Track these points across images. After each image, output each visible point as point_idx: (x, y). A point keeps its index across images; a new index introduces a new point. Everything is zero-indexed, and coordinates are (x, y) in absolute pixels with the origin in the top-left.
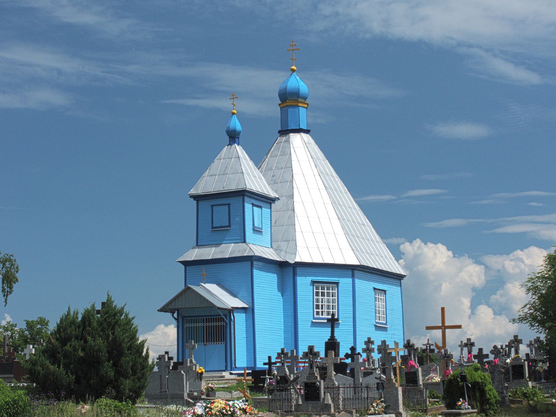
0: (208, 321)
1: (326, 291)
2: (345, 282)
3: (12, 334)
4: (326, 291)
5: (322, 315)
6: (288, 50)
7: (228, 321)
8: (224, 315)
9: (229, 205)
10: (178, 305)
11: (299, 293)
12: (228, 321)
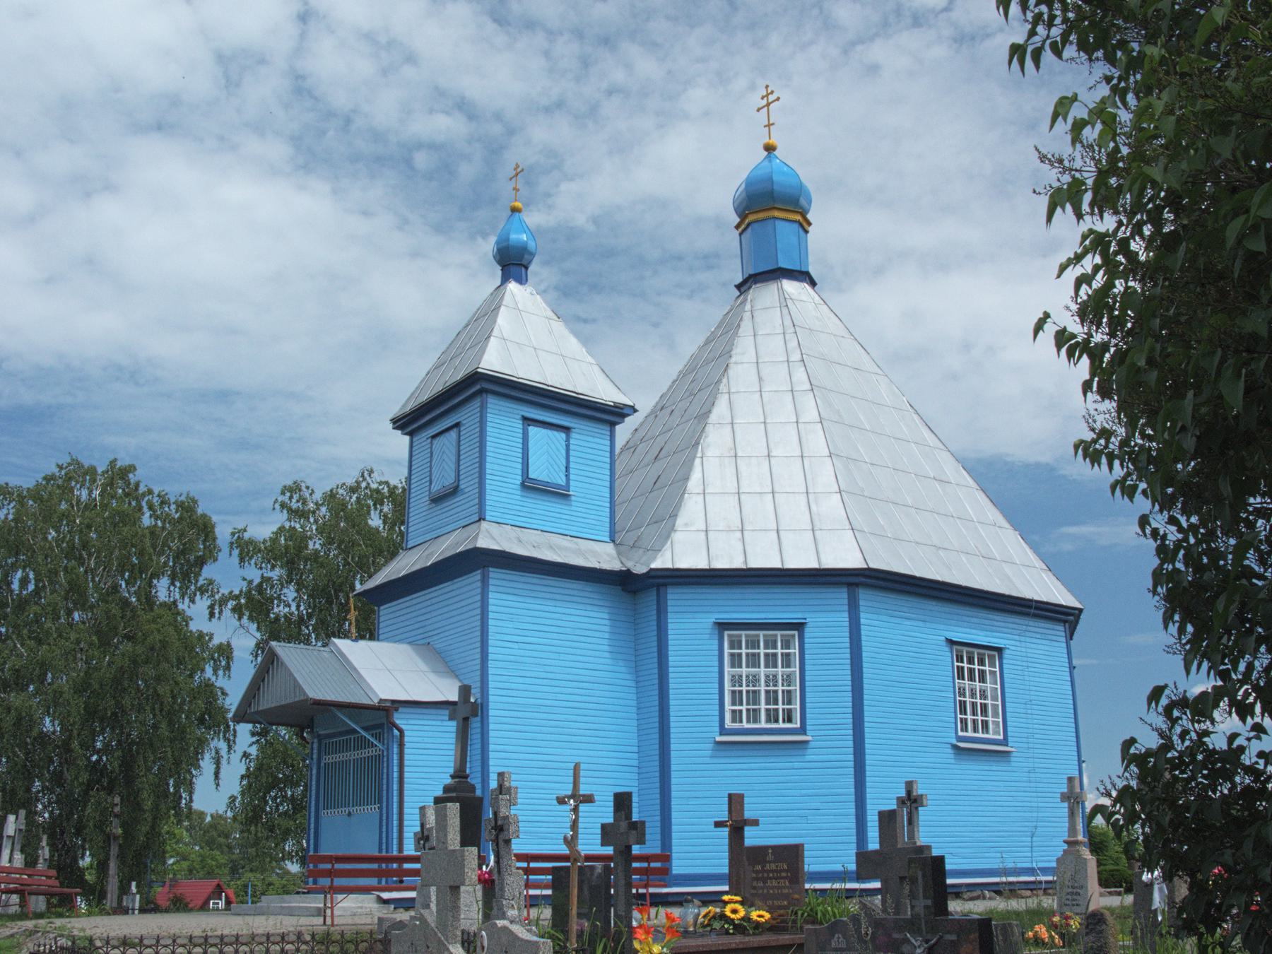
2: (826, 620)
6: (758, 110)
9: (457, 425)
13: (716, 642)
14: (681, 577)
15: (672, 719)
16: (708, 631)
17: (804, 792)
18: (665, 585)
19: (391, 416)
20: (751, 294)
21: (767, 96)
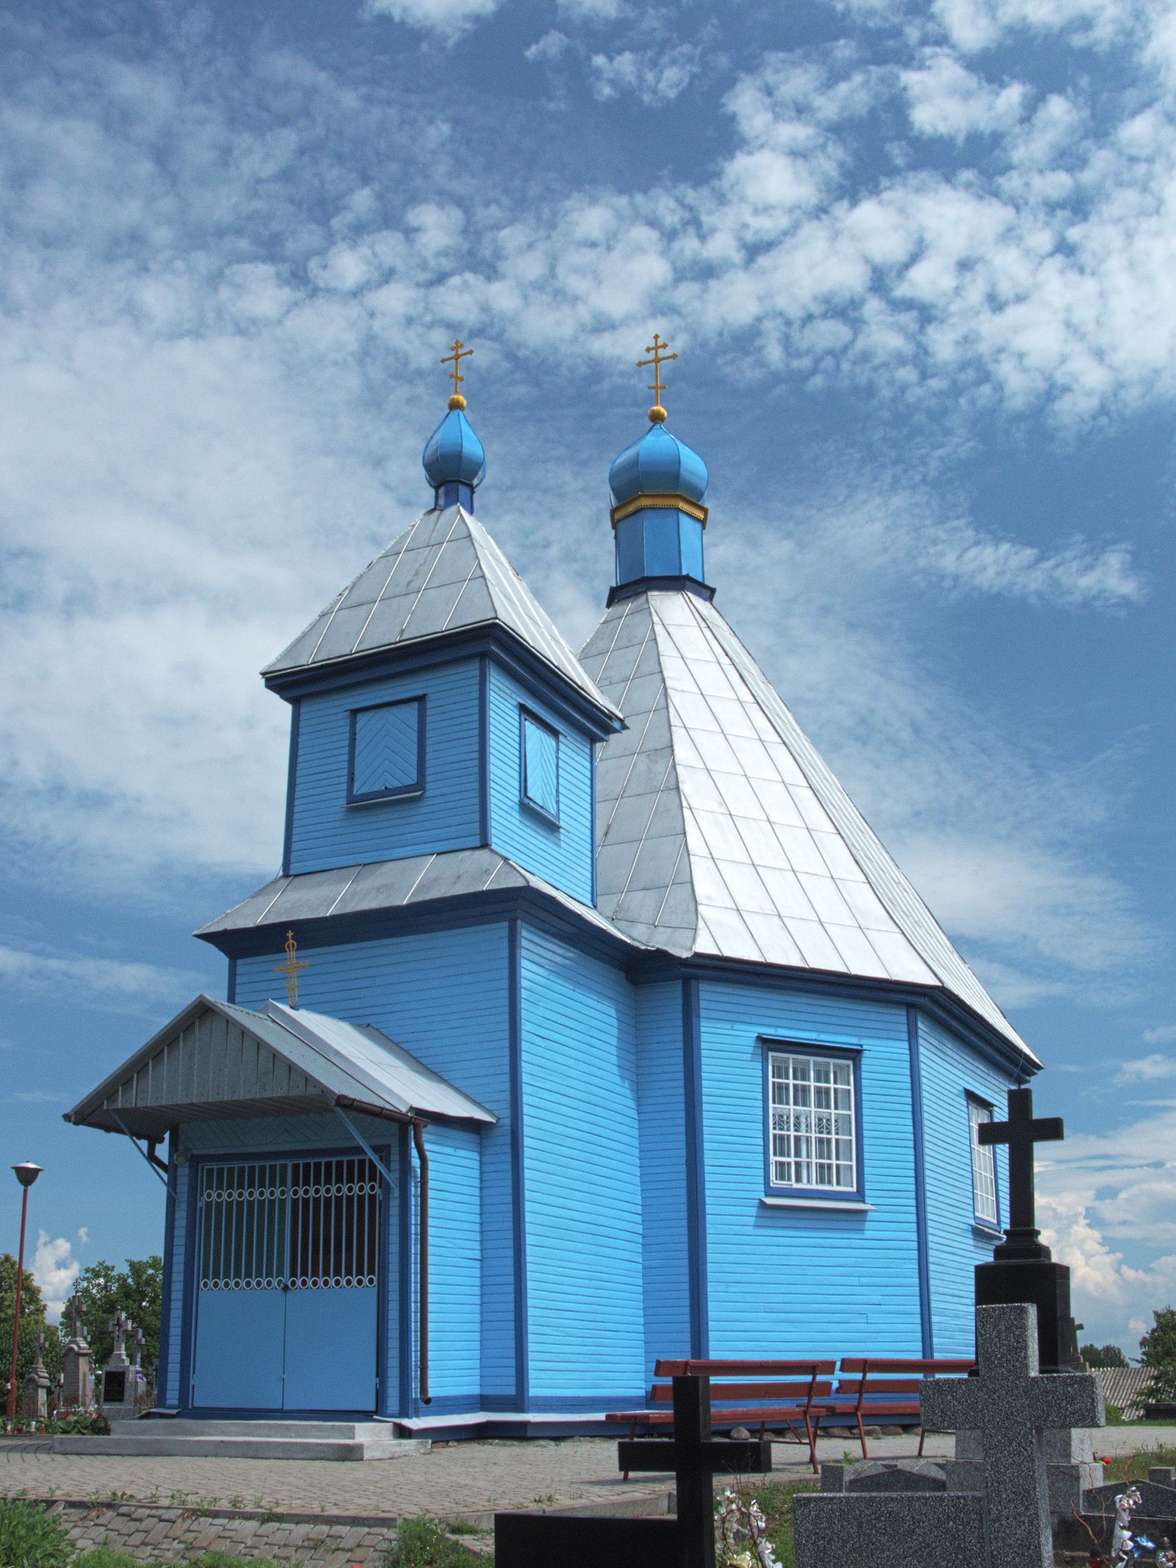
0: (304, 1176)
1: (812, 1084)
3: (106, 1282)
4: (812, 1084)
5: (798, 1179)
7: (392, 1178)
8: (375, 1149)
9: (421, 699)
10: (156, 1092)
11: (708, 1085)
12: (392, 1178)
13: (759, 1066)
14: (778, 977)
15: (707, 1169)
16: (751, 1050)
17: (864, 1280)
18: (698, 978)
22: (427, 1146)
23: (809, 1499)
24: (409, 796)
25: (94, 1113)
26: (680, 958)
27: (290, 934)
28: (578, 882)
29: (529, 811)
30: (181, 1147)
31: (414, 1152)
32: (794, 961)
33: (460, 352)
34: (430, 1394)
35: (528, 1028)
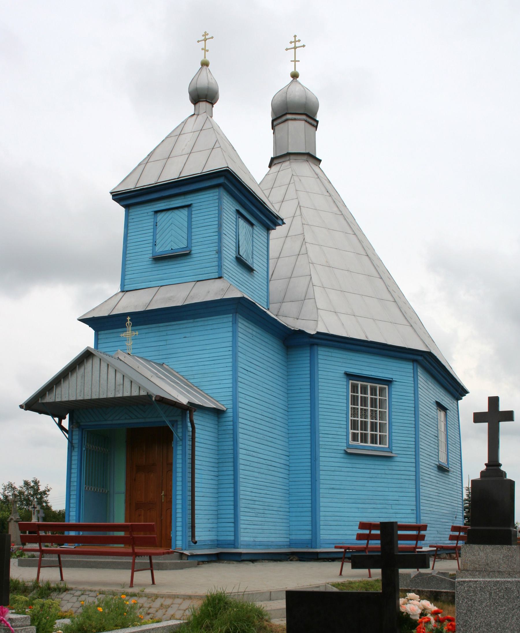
9: (189, 206)
10: (67, 393)
18: (318, 345)
19: (111, 189)
20: (158, 214)
21: (295, 42)
22: (195, 421)
23: (464, 582)
24: (184, 255)
25: (36, 404)
26: (310, 334)
27: (129, 318)
28: (261, 297)
29: (240, 261)
30: (74, 421)
31: (189, 424)
32: (363, 338)
33: (207, 37)
34: (197, 539)
35: (241, 366)
